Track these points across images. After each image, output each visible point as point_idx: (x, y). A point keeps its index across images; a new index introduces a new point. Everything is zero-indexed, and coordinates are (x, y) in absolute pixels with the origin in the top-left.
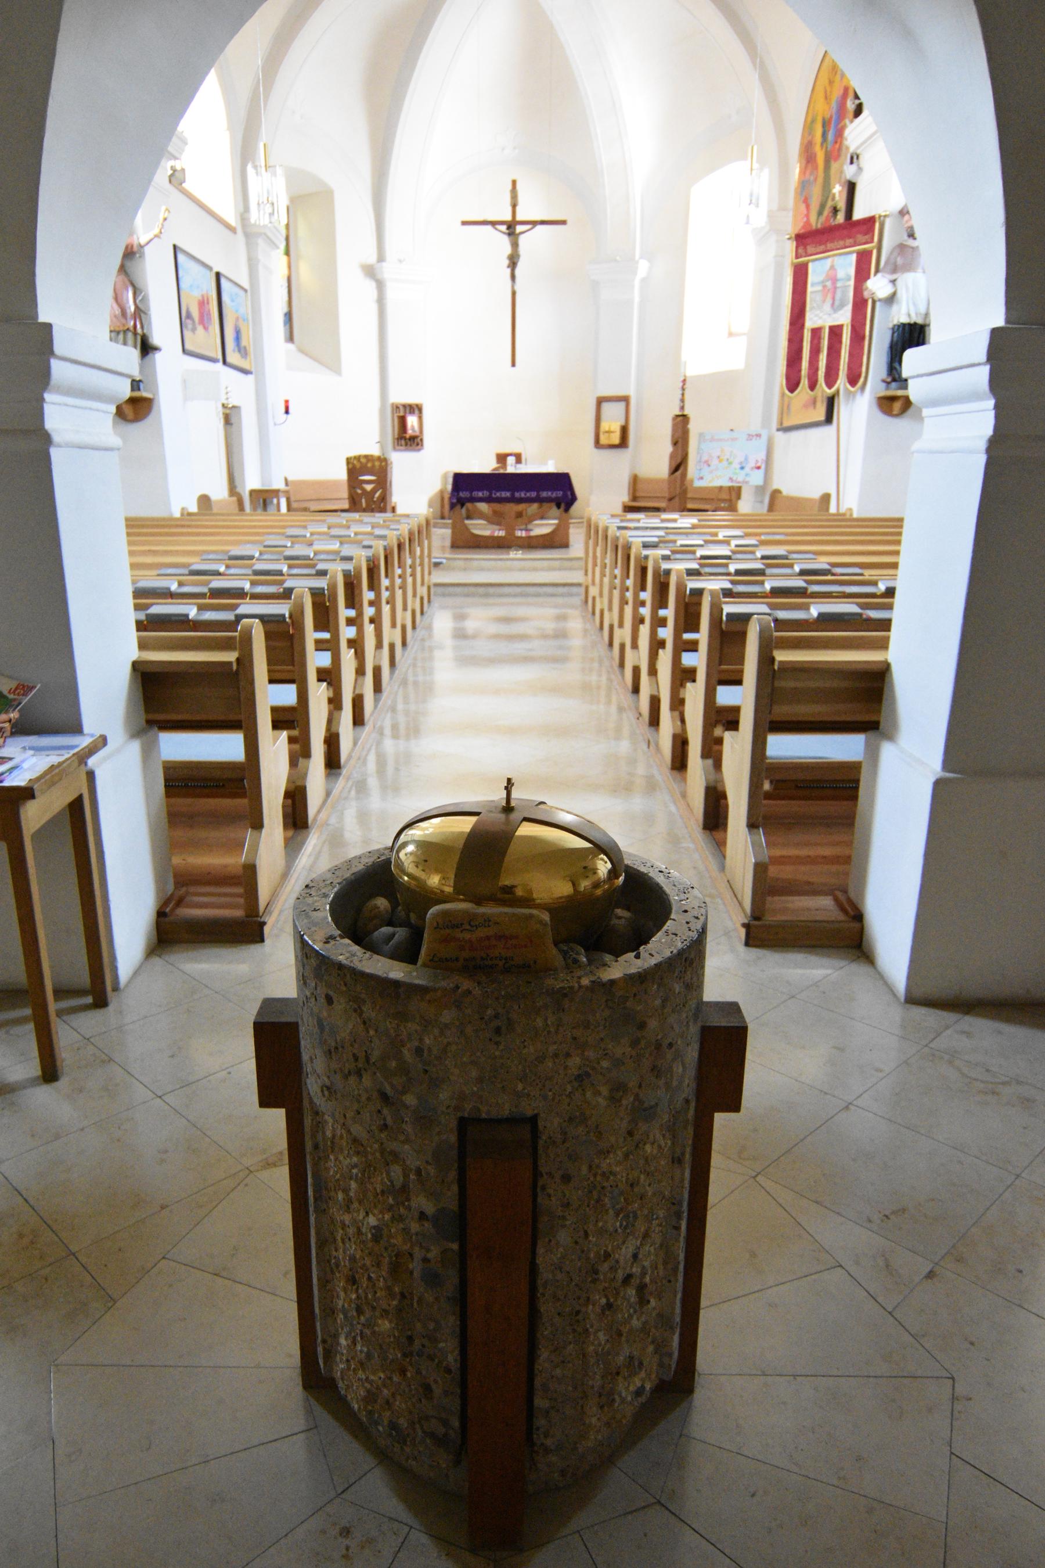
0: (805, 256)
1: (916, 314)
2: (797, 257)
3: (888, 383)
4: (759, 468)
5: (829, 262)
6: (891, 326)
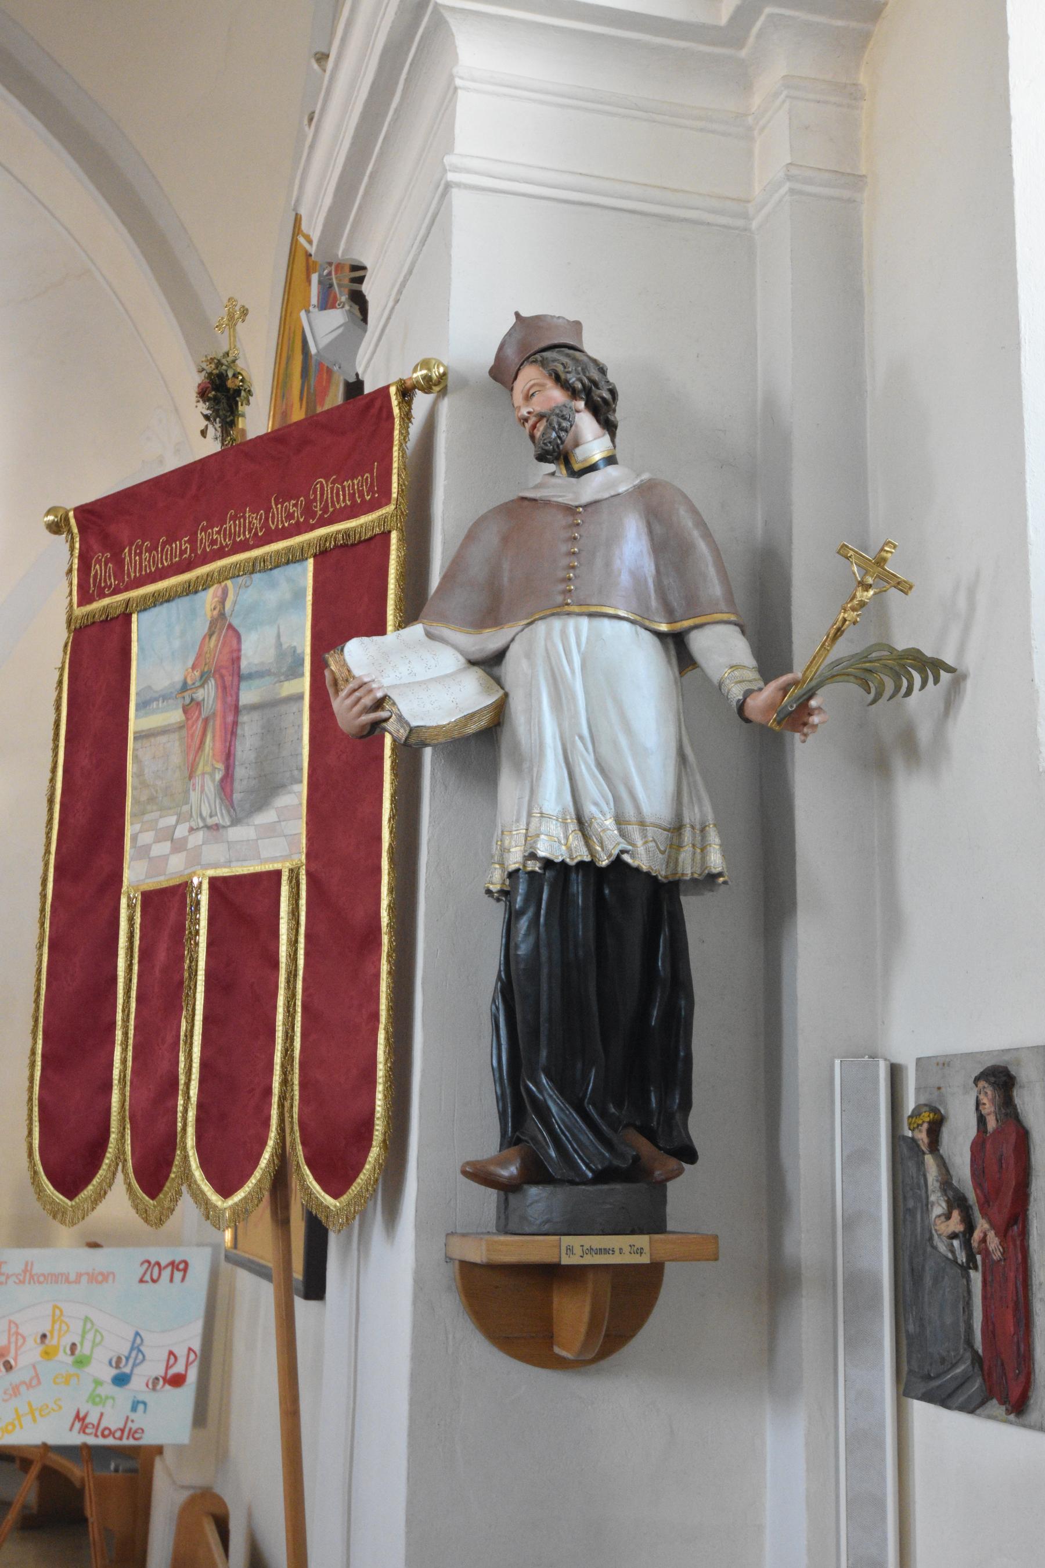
0: (116, 591)
1: (620, 821)
2: (85, 598)
3: (508, 1189)
4: (177, 1381)
5: (209, 598)
6: (496, 880)
